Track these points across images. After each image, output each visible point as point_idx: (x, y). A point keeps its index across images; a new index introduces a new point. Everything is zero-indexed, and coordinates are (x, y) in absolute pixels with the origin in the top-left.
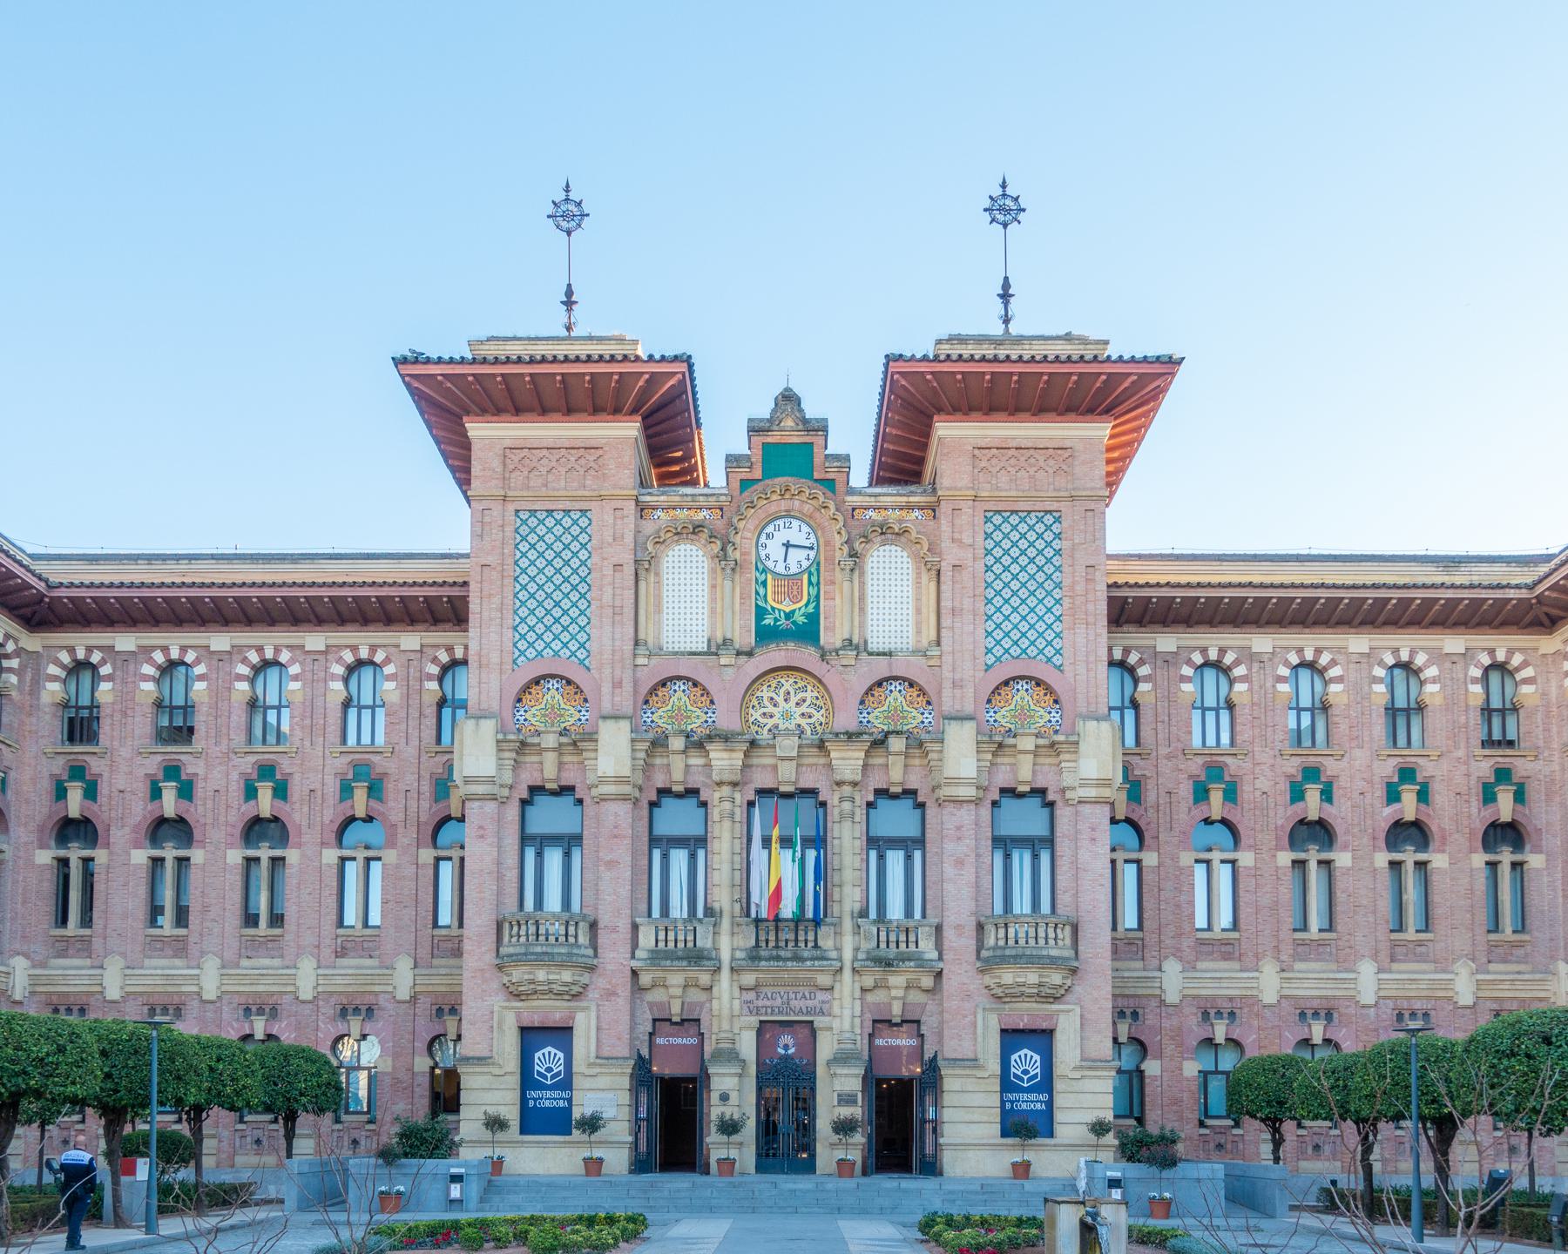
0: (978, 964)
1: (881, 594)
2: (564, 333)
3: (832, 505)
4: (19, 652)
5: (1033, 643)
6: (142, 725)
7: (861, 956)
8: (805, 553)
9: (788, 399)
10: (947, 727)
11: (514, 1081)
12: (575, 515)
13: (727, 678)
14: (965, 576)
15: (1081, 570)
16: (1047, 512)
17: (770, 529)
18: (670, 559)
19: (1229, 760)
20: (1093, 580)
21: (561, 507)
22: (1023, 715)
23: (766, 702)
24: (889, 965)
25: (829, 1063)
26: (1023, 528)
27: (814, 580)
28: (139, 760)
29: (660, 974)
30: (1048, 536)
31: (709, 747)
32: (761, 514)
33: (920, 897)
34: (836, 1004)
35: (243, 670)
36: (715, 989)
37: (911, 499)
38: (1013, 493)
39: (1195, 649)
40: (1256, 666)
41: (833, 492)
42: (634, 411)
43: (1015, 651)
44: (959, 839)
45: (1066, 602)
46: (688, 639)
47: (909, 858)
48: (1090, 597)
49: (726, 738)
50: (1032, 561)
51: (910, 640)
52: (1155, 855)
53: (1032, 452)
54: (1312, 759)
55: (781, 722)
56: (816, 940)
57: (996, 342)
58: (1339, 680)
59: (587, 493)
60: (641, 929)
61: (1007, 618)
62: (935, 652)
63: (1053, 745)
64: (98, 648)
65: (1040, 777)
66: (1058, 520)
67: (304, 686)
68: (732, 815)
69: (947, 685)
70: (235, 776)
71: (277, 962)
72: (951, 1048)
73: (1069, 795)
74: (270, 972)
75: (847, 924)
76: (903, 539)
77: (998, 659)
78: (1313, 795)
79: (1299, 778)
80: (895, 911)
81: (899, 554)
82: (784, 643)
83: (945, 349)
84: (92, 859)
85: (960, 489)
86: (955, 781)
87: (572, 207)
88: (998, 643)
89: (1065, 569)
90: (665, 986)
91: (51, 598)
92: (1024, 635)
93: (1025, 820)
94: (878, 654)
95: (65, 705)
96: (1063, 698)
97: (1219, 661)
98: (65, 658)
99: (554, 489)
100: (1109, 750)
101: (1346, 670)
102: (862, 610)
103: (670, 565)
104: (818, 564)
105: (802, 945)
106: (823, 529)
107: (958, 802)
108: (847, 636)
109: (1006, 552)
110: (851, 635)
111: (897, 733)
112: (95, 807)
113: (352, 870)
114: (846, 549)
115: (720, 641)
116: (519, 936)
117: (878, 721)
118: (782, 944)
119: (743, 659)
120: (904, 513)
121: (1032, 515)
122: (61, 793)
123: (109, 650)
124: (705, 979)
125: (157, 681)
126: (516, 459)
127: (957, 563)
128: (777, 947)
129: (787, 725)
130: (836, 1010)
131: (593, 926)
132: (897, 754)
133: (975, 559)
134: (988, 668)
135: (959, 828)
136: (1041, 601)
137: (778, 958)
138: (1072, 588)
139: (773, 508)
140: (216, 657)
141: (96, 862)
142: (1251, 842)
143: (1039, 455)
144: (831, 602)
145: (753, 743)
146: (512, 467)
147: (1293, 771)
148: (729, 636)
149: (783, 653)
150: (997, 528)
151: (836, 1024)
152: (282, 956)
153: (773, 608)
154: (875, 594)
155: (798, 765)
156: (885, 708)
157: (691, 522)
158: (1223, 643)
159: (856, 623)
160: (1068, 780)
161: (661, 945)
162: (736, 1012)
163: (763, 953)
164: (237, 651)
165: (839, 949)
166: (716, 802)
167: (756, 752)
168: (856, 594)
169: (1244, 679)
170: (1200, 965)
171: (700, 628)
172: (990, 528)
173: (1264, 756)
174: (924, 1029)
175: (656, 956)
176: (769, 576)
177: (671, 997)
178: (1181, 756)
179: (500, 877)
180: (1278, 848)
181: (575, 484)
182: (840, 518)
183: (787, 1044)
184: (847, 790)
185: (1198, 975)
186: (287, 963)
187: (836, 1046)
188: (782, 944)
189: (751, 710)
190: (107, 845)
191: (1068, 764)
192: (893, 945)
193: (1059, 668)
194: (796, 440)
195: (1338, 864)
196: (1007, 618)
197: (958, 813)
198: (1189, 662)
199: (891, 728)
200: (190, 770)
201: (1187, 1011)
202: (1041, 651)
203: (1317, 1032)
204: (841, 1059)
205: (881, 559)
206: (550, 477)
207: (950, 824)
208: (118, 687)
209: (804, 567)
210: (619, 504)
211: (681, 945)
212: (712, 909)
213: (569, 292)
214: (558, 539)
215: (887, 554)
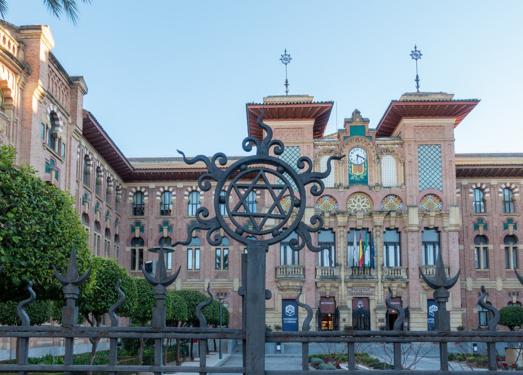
0: (420, 280)
1: (386, 170)
2: (285, 94)
3: (371, 144)
4: (122, 188)
5: (433, 184)
6: (157, 210)
7: (384, 277)
8: (362, 159)
9: (357, 113)
10: (409, 209)
11: (281, 315)
12: (291, 148)
13: (341, 195)
14: (413, 164)
15: (448, 163)
16: (436, 145)
17: (352, 151)
18: (323, 160)
19: (485, 217)
20: (452, 165)
21: (291, 145)
22: (430, 205)
23: (352, 202)
24: (393, 280)
25: (375, 310)
26: (429, 150)
27: (366, 166)
28: (156, 220)
29: (324, 283)
30: (437, 152)
31: (337, 216)
32: (350, 147)
33: (401, 261)
34: (376, 292)
35: (187, 193)
36: (340, 288)
37: (395, 142)
38: (427, 140)
39: (473, 184)
40: (492, 189)
41: (372, 140)
42: (314, 117)
43: (428, 186)
44: (413, 242)
45: (443, 172)
46: (329, 184)
47: (395, 248)
48: (451, 170)
49: (343, 213)
50: (432, 159)
51: (395, 183)
52: (463, 246)
53: (432, 127)
54: (510, 216)
55: (357, 208)
56: (370, 273)
57: (415, 94)
58: (518, 192)
59: (299, 141)
60: (318, 270)
61: (425, 176)
62: (404, 187)
63: (440, 214)
64: (144, 187)
65: (436, 224)
66: (440, 147)
67: (205, 198)
68: (344, 236)
69: (408, 197)
70: (185, 224)
71: (198, 280)
72: (412, 305)
73: (445, 229)
74: (196, 283)
75: (379, 268)
76: (393, 153)
77: (423, 189)
78: (511, 227)
79: (506, 222)
80: (392, 264)
81: (391, 158)
82: (359, 185)
83: (405, 98)
84: (143, 250)
85: (410, 139)
86: (412, 225)
87: (287, 56)
88: (423, 184)
89: (443, 162)
90: (325, 287)
91: (134, 173)
92: (430, 181)
93: (432, 236)
94: (387, 188)
95: (133, 204)
96: (443, 200)
97: (481, 187)
98: (134, 190)
99: (289, 140)
100: (459, 215)
101: (520, 189)
102: (381, 175)
103: (323, 162)
104: (367, 161)
105: (366, 274)
106: (368, 151)
107: (413, 231)
108: (377, 182)
109: (425, 157)
110: (378, 182)
111: (393, 211)
112: (143, 234)
113: (190, 252)
114: (376, 157)
115: (338, 184)
116: (283, 272)
117: (386, 207)
118: (360, 274)
119: (346, 189)
120: (393, 146)
121: (432, 146)
122: (133, 230)
123: (147, 188)
124: (337, 285)
125: (161, 196)
126: (278, 132)
127: (410, 160)
128: (358, 275)
129: (359, 209)
130: (376, 294)
131: (304, 269)
132: (393, 217)
133: (415, 159)
134: (420, 191)
135: (413, 239)
136: (435, 171)
137: (359, 278)
138: (445, 167)
139: (353, 145)
140: (179, 190)
141: (144, 250)
142: (492, 242)
143: (433, 128)
144: (371, 172)
145: (350, 215)
146: (276, 134)
147: (504, 220)
148: (341, 183)
149: (358, 188)
150: (422, 150)
151: (376, 298)
152: (199, 278)
153: (354, 174)
154: (384, 170)
155: (363, 221)
156: (388, 204)
157: (329, 149)
158: (482, 182)
159: (379, 179)
160: (445, 224)
161: (323, 274)
162: (346, 295)
163: (354, 277)
164: (185, 188)
165: (377, 276)
166: (338, 232)
167: (351, 217)
168: (379, 170)
169: (488, 192)
170: (477, 279)
171: (332, 180)
172: (419, 150)
173: (495, 216)
174: (402, 299)
175: (323, 278)
176: (352, 165)
177: (326, 290)
178: (470, 216)
179: (275, 255)
180: (501, 243)
181: (295, 139)
182: (374, 147)
183: (360, 305)
184: (378, 228)
185: (477, 282)
186: (201, 280)
187: (376, 305)
188: (360, 274)
189: (348, 205)
190: (147, 245)
191: (445, 220)
192: (393, 274)
193: (442, 191)
194: (360, 125)
195: (519, 248)
196: (425, 176)
197: (413, 235)
198: (472, 188)
199: (390, 210)
200: (171, 223)
201: (474, 293)
202: (436, 186)
203: (514, 300)
204: (378, 308)
205: (386, 160)
206: (288, 137)
207: (410, 238)
208: (150, 198)
209: (363, 162)
210: (308, 144)
211: (329, 275)
212: (338, 264)
213: (287, 82)
214: (290, 155)
215: (388, 158)
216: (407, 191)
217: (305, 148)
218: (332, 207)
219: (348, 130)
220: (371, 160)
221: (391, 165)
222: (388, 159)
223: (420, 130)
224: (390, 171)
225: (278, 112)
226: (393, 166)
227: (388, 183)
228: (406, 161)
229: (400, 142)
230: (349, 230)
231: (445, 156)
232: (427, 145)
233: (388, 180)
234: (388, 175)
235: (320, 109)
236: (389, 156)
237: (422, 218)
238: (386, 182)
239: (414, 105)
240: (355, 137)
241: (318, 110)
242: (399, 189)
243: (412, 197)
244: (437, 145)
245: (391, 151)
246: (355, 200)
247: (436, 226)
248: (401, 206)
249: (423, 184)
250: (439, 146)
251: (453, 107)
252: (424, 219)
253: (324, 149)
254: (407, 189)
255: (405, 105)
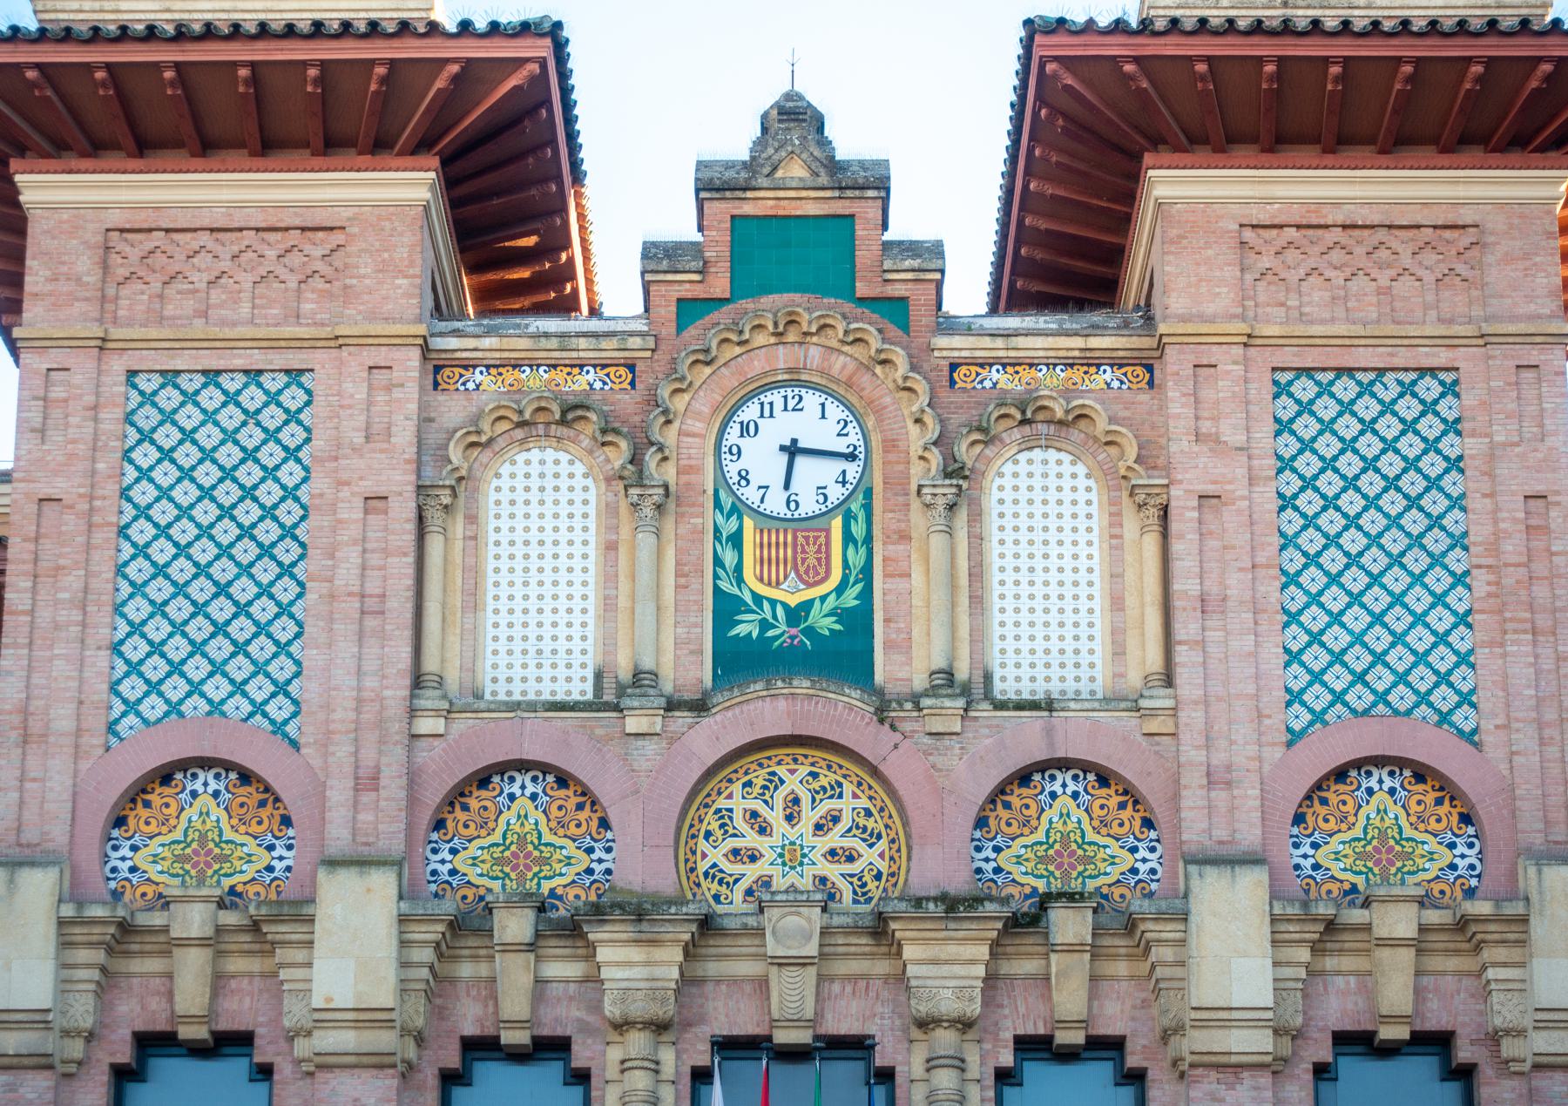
3: (900, 357)
10: (1195, 883)
14: (1231, 519)
16: (1423, 371)
17: (750, 412)
21: (239, 363)
26: (1367, 408)
27: (858, 530)
37: (1094, 342)
38: (1341, 329)
41: (905, 328)
42: (421, 146)
43: (1359, 698)
45: (1480, 580)
46: (547, 673)
51: (1098, 673)
53: (1381, 235)
55: (776, 871)
61: (1336, 618)
63: (1462, 924)
65: (1433, 1004)
66: (1451, 389)
69: (1193, 779)
73: (1509, 1048)
76: (1075, 434)
77: (1318, 717)
81: (1067, 469)
82: (788, 680)
86: (1221, 1017)
88: (1317, 677)
92: (1379, 658)
96: (1485, 811)
99: (223, 323)
102: (978, 601)
103: (505, 496)
104: (869, 493)
106: (879, 412)
108: (939, 662)
110: (952, 659)
115: (625, 675)
119: (682, 719)
120: (1076, 374)
121: (1389, 378)
126: (134, 254)
127: (1210, 489)
129: (793, 878)
132: (1070, 949)
133: (1252, 481)
134: (1294, 738)
138: (1494, 547)
139: (757, 365)
143: (1394, 240)
144: (900, 584)
145: (707, 925)
146: (122, 272)
148: (648, 663)
149: (782, 704)
150: (1306, 408)
153: (757, 598)
155: (821, 978)
156: (1040, 835)
157: (557, 396)
159: (964, 631)
166: (612, 1072)
167: (716, 946)
171: (577, 645)
172: (1287, 408)
176: (748, 524)
182: (921, 386)
184: (945, 1039)
189: (703, 845)
191: (1502, 973)
193: (1471, 738)
194: (812, 209)
196: (1336, 618)
199: (1056, 885)
202: (1424, 698)
206: (216, 296)
210: (380, 356)
214: (230, 437)
215: (1037, 469)
216: (1185, 737)
217: (348, 386)
218: (568, 861)
219: (718, 250)
220: (897, 484)
221: (1067, 523)
222: (1037, 482)
223: (1291, 255)
224: (1054, 577)
225: (324, 99)
226: (1082, 537)
227: (1040, 673)
228: (1175, 492)
229: (1135, 342)
230: (1007, 1058)
231: (1491, 456)
232: (1350, 371)
233: (1040, 645)
234: (1039, 604)
235: (455, 79)
236: (1052, 455)
237: (1304, 954)
238: (1026, 659)
239: (1209, 59)
240: (767, 301)
241: (440, 84)
242: (1127, 721)
243: (1229, 784)
244: (1432, 371)
245: (1059, 414)
246: (758, 806)
247: (1434, 1021)
248: (1147, 859)
249: (1317, 677)
250: (1448, 377)
251: (1527, 77)
252: (1330, 963)
253: (517, 391)
254: (1183, 715)
255: (1137, 60)
